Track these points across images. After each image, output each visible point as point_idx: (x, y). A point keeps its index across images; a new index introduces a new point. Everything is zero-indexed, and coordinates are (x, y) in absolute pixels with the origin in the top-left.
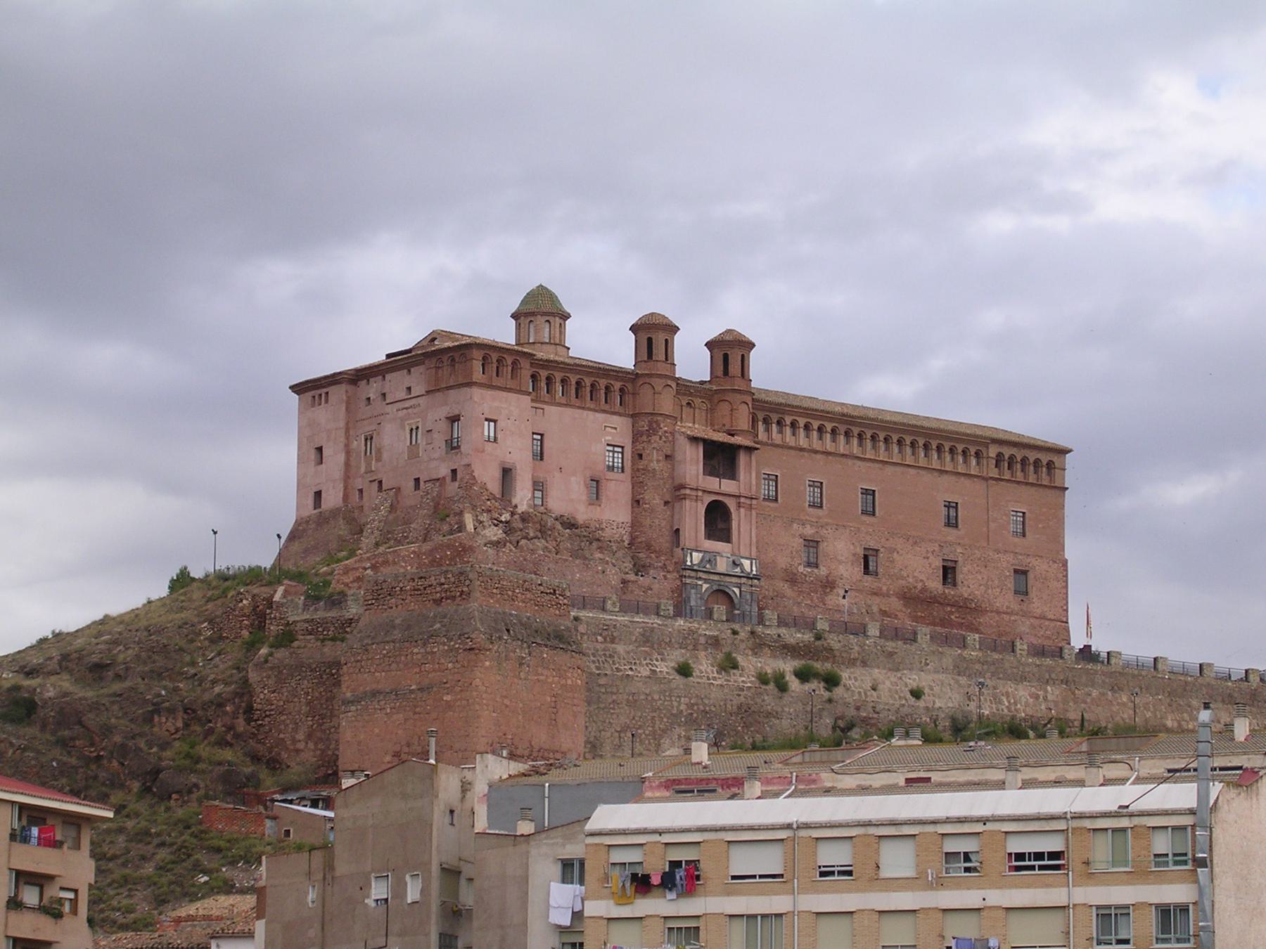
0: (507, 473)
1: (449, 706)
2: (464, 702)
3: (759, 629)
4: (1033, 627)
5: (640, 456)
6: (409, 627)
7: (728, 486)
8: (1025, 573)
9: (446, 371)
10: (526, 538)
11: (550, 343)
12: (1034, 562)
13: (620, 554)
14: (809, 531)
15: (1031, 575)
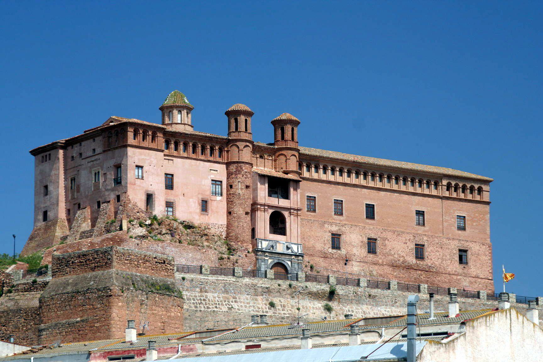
0: (149, 198)
2: (106, 327)
3: (294, 283)
4: (471, 283)
5: (231, 187)
6: (76, 284)
7: (283, 203)
8: (466, 251)
9: (114, 139)
10: (160, 234)
11: (181, 124)
13: (219, 243)
14: (334, 229)
15: (469, 253)
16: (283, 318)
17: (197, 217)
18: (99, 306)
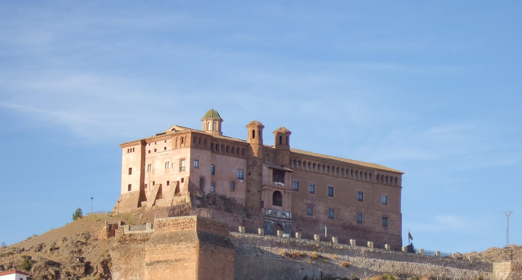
5: (250, 174)
8: (386, 218)
14: (309, 202)
16: (288, 262)
18: (187, 253)
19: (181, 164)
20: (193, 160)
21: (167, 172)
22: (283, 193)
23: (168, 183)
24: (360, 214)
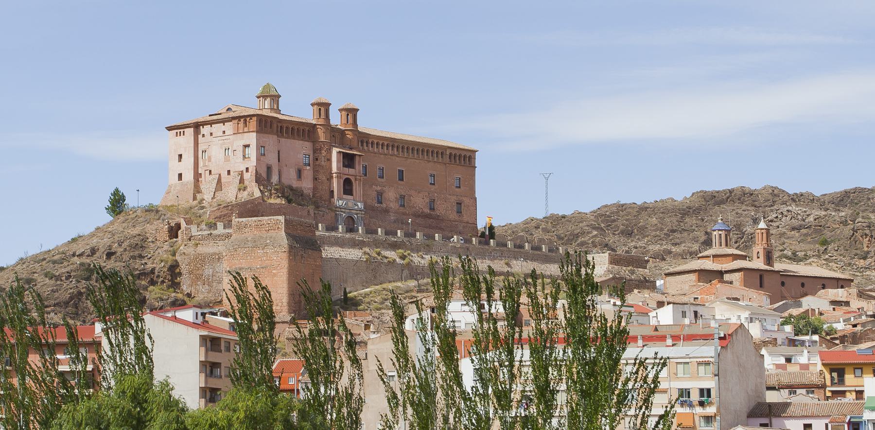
1: (275, 275)
7: (351, 171)
12: (464, 199)
14: (379, 188)
17: (294, 182)
19: (244, 152)
20: (260, 146)
21: (227, 159)
22: (353, 181)
23: (229, 172)
24: (433, 201)
